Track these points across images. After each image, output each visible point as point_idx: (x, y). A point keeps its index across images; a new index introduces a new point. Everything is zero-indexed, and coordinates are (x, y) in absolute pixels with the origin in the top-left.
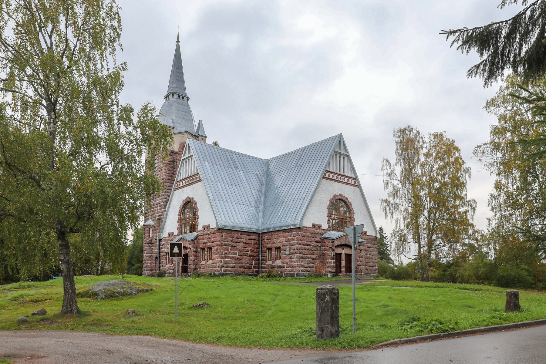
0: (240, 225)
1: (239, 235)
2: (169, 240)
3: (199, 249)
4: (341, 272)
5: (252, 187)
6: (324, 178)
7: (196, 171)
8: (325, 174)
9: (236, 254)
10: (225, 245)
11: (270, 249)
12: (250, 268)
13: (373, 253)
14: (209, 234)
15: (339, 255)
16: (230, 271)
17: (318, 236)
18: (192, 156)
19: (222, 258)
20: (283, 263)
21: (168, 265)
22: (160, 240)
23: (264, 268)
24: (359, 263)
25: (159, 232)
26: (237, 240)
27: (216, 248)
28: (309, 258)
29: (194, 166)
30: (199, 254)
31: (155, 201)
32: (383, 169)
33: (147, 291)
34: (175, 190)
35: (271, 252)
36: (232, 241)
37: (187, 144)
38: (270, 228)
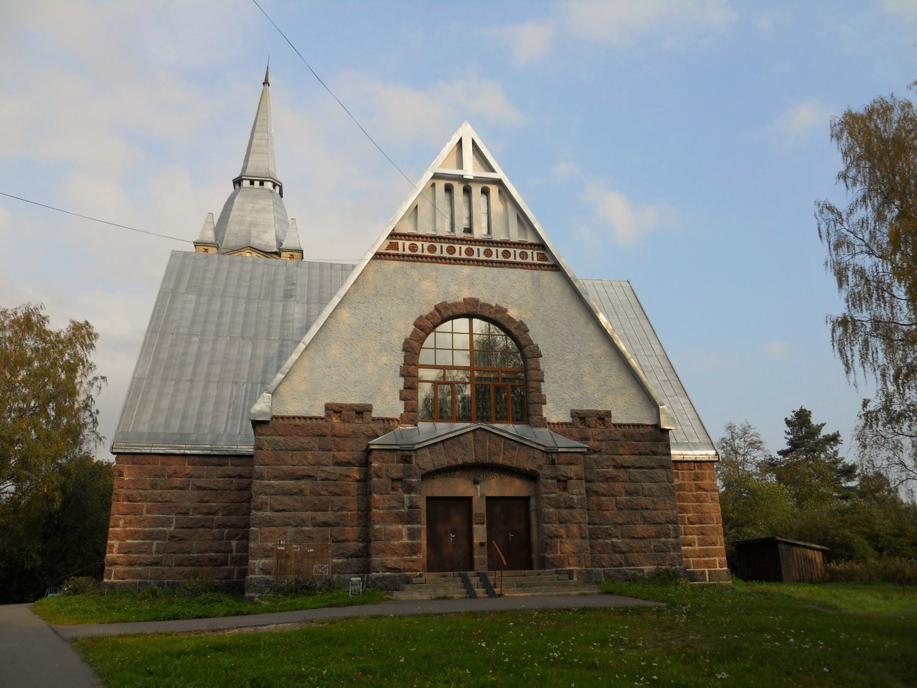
8: (394, 246)
9: (168, 523)
13: (647, 485)
17: (350, 443)
28: (303, 523)
36: (154, 486)
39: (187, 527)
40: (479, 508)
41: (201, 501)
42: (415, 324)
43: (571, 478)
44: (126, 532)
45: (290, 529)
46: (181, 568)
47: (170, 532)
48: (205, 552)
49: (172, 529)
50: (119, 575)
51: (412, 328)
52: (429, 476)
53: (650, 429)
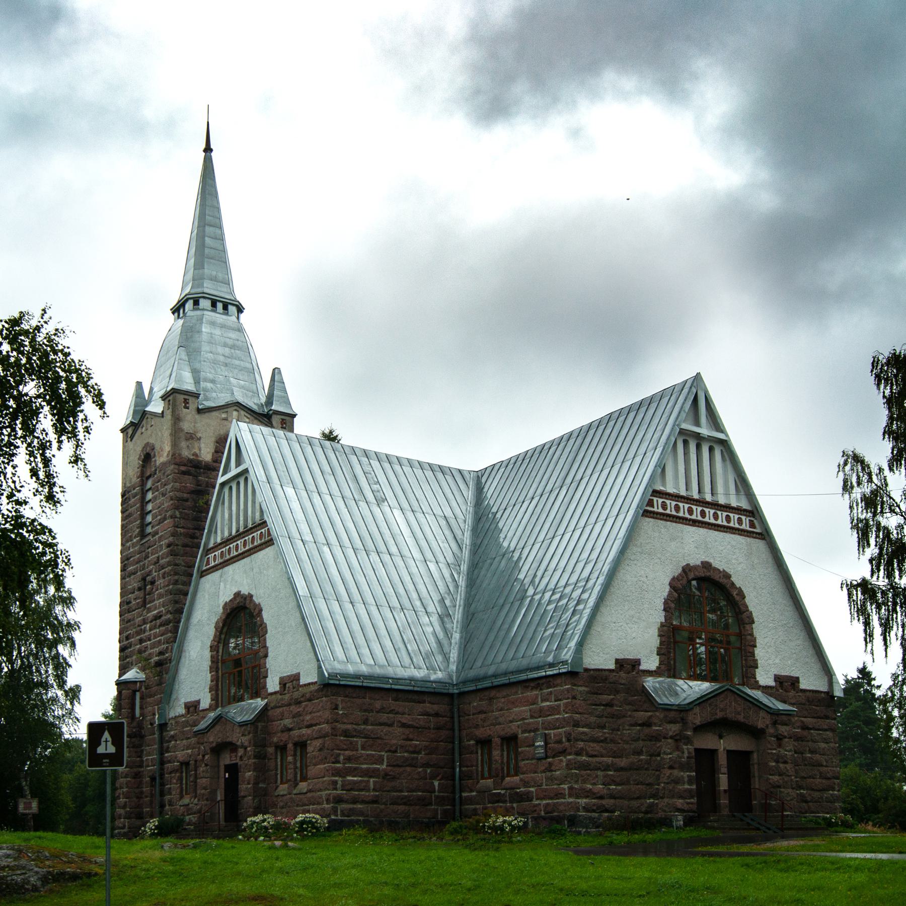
0: (390, 671)
1: (390, 703)
2: (186, 724)
3: (271, 750)
4: (715, 808)
5: (429, 555)
6: (647, 514)
7: (258, 514)
8: (650, 503)
9: (380, 760)
10: (346, 734)
11: (485, 743)
12: (424, 802)
13: (823, 745)
14: (298, 703)
15: (705, 758)
16: (361, 813)
18: (246, 471)
19: (337, 772)
20: (526, 784)
21: (186, 800)
22: (163, 727)
23: (470, 801)
24: (775, 778)
25: (159, 702)
26: (384, 717)
27: (318, 743)
28: (607, 768)
29: (254, 502)
30: (272, 764)
31: (149, 610)
32: (847, 487)
33: (74, 877)
34: (203, 574)
35: (490, 754)
36: (366, 722)
37: (231, 437)
38: (485, 678)
39: (398, 766)
40: (722, 760)
41: (408, 739)
42: (670, 584)
43: (785, 737)
44: (346, 768)
45: (600, 773)
46: (395, 807)
47: (383, 770)
48: (413, 791)
49: (384, 767)
50: (346, 812)
51: (668, 589)
52: (698, 729)
53: (823, 695)
